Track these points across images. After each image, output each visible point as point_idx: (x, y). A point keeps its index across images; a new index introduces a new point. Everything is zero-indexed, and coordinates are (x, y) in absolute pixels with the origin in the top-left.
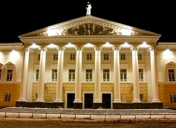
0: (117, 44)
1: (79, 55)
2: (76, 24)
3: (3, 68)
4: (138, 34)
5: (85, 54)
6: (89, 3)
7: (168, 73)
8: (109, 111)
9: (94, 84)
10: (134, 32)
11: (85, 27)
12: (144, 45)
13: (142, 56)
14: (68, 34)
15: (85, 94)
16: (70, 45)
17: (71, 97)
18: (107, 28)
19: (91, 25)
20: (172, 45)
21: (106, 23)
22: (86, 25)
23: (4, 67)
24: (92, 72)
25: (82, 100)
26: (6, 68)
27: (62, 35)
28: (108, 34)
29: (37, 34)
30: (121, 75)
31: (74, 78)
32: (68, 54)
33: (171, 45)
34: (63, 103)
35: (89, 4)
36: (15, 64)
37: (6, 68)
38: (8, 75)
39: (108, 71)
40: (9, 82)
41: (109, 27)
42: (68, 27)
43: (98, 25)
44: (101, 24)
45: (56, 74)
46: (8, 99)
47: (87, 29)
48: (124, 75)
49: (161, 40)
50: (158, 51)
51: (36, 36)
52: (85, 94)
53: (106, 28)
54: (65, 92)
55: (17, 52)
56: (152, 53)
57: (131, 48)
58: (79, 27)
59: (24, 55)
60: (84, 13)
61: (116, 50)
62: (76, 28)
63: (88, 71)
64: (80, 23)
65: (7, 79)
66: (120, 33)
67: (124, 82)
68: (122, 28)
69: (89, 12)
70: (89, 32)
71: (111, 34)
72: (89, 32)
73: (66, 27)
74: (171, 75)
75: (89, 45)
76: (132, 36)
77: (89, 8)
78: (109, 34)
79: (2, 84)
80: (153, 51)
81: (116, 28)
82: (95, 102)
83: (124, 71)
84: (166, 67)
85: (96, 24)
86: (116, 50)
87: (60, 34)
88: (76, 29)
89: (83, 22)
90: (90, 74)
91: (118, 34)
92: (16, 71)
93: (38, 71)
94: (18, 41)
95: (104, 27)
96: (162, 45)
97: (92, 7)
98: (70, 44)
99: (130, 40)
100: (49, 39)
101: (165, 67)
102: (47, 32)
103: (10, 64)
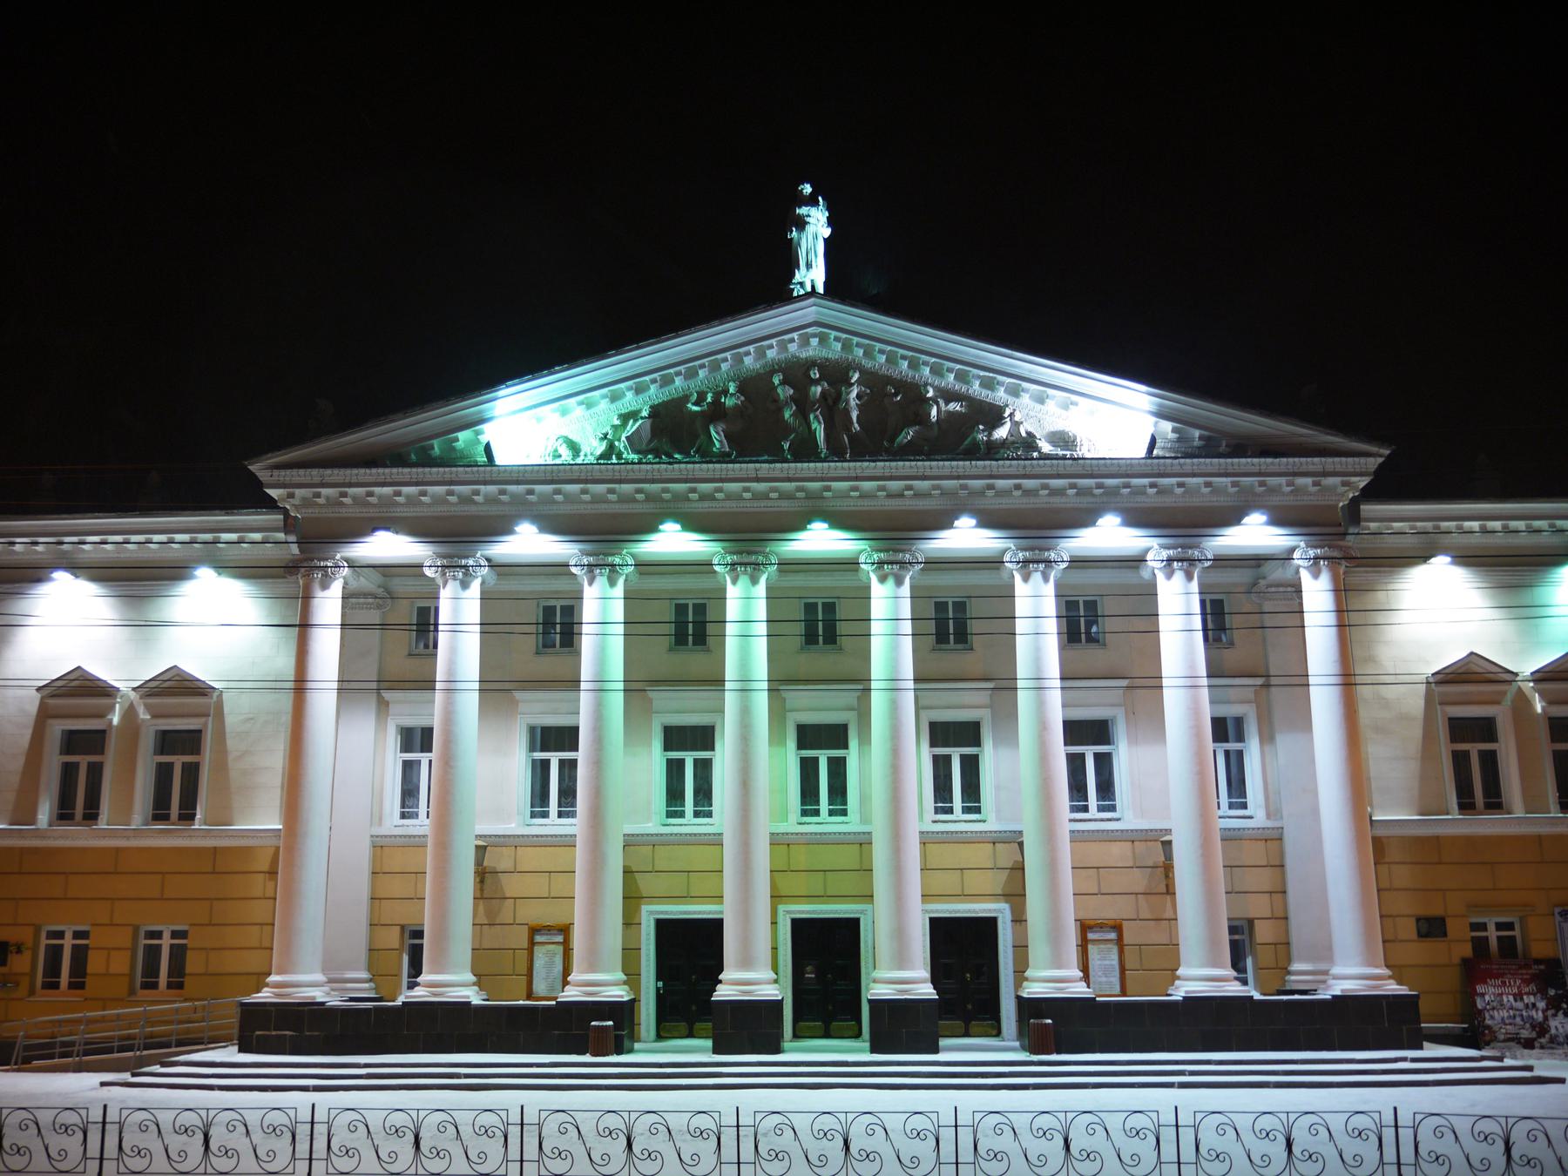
2: (715, 367)
3: (116, 720)
4: (1197, 443)
6: (807, 189)
7: (1445, 749)
10: (1167, 426)
11: (785, 392)
13: (1244, 619)
16: (672, 541)
19: (836, 374)
21: (949, 362)
22: (797, 373)
23: (130, 712)
26: (143, 715)
34: (633, 1001)
35: (812, 201)
37: (143, 715)
39: (968, 733)
41: (976, 389)
42: (655, 394)
46: (163, 978)
47: (803, 405)
49: (1384, 487)
53: (950, 396)
56: (1317, 594)
58: (740, 390)
62: (716, 402)
63: (676, 738)
68: (1074, 398)
69: (812, 274)
71: (993, 450)
73: (639, 390)
75: (820, 540)
76: (1150, 467)
78: (973, 452)
83: (954, 736)
85: (868, 364)
88: (716, 412)
92: (231, 743)
95: (931, 394)
96: (1395, 519)
97: (830, 222)
103: (177, 687)
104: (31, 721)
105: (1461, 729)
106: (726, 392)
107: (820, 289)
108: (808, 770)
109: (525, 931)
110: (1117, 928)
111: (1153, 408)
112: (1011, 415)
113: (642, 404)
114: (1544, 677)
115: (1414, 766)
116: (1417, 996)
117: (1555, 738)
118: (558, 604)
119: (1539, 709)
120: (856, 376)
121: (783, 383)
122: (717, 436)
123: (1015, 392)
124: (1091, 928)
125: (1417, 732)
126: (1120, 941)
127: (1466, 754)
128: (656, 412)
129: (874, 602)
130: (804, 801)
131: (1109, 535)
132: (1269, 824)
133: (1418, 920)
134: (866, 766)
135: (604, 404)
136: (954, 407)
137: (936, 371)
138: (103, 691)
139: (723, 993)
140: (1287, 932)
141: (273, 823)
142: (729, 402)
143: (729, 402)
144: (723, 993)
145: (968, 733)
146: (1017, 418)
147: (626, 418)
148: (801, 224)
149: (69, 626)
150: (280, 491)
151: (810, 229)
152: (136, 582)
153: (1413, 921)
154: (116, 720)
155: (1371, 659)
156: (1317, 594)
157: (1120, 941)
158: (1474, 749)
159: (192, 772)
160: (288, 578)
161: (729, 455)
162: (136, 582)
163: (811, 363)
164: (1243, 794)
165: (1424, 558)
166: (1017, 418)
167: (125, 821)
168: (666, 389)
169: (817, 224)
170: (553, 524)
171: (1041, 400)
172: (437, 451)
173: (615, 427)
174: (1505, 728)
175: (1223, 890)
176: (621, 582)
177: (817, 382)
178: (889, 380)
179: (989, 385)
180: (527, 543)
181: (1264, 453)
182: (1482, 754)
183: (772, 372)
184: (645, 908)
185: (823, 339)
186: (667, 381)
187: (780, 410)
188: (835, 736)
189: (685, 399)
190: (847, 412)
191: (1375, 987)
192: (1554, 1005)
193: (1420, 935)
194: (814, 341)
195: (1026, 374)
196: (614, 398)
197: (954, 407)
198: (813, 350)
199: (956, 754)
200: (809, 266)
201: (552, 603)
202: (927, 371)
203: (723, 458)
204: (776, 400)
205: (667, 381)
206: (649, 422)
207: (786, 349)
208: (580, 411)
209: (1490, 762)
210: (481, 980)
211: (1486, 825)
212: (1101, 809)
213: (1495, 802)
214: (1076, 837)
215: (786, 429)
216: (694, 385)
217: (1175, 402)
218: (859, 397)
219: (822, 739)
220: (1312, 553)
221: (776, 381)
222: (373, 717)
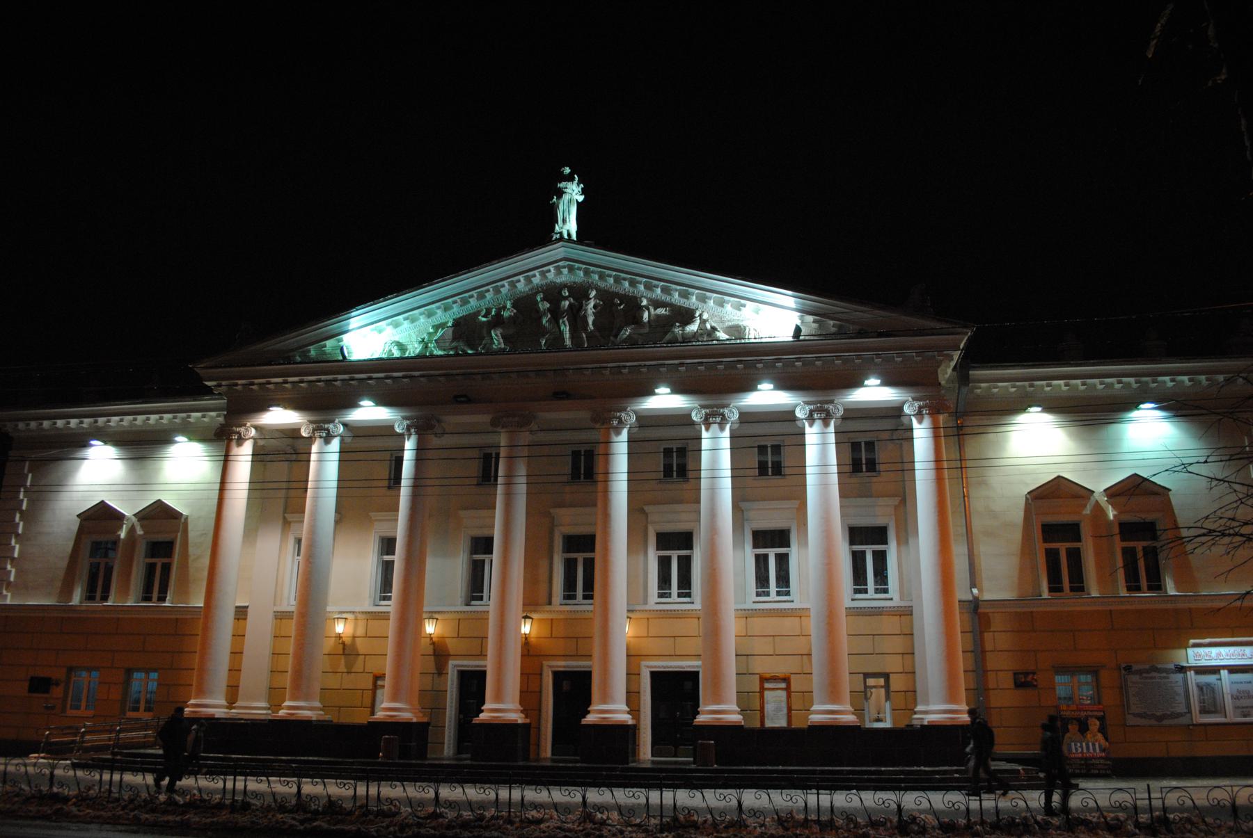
1: (715, 450)
2: (497, 291)
3: (123, 535)
4: (833, 330)
5: (747, 442)
6: (567, 170)
7: (1040, 547)
8: (363, 764)
9: (799, 614)
10: (810, 318)
12: (873, 392)
13: (870, 453)
14: (455, 348)
15: (652, 673)
16: (873, 392)
17: (575, 689)
19: (580, 293)
20: (1062, 382)
21: (655, 282)
22: (553, 293)
23: (132, 530)
24: (885, 542)
26: (140, 532)
27: (420, 357)
28: (668, 337)
29: (293, 350)
30: (858, 559)
31: (685, 582)
32: (470, 453)
33: (1160, 378)
34: (526, 727)
35: (570, 178)
36: (185, 512)
37: (140, 532)
38: (151, 569)
39: (877, 535)
41: (676, 298)
42: (457, 311)
43: (613, 289)
44: (617, 280)
47: (556, 313)
48: (584, 571)
49: (976, 356)
50: (966, 421)
51: (289, 361)
52: (652, 673)
53: (657, 304)
54: (446, 663)
55: (1048, 418)
56: (922, 436)
57: (907, 410)
58: (514, 306)
59: (226, 462)
60: (540, 230)
61: (715, 427)
62: (498, 314)
63: (667, 540)
64: (521, 286)
65: (473, 591)
66: (737, 331)
67: (871, 598)
68: (743, 302)
70: (567, 335)
71: (687, 339)
72: (567, 335)
73: (446, 309)
74: (1140, 554)
75: (279, 417)
76: (798, 346)
80: (927, 422)
81: (711, 303)
83: (866, 536)
85: (602, 284)
86: (715, 427)
87: (414, 349)
88: (498, 321)
89: (537, 280)
90: (874, 552)
91: (722, 335)
92: (191, 550)
94: (195, 389)
95: (645, 302)
96: (995, 381)
97: (584, 192)
98: (663, 390)
99: (790, 364)
100: (269, 383)
101: (1022, 514)
102: (344, 337)
103: (160, 514)
104: (73, 536)
105: (1051, 532)
106: (504, 308)
107: (574, 237)
108: (761, 561)
109: (371, 677)
110: (786, 680)
111: (799, 307)
112: (701, 315)
113: (448, 318)
114: (1114, 493)
115: (1015, 561)
116: (428, 724)
118: (583, 449)
119: (1111, 517)
120: (593, 293)
121: (543, 299)
123: (703, 300)
124: (768, 680)
125: (1018, 536)
126: (788, 689)
127: (1057, 552)
128: (457, 323)
129: (728, 446)
130: (660, 588)
131: (766, 396)
132: (903, 604)
134: (804, 559)
135: (422, 319)
136: (661, 311)
137: (649, 287)
138: (117, 517)
139: (701, 719)
140: (914, 681)
141: (200, 603)
142: (506, 314)
143: (506, 314)
144: (701, 719)
145: (877, 535)
146: (705, 316)
147: (437, 327)
148: (560, 193)
149: (98, 473)
150: (214, 383)
151: (566, 197)
152: (141, 447)
153: (1010, 675)
154: (123, 535)
155: (983, 483)
156: (922, 436)
157: (788, 689)
158: (1063, 547)
159: (167, 568)
160: (222, 438)
161: (504, 350)
162: (141, 447)
163: (564, 286)
164: (788, 585)
165: (1022, 409)
166: (705, 316)
167: (126, 598)
168: (464, 308)
169: (574, 192)
171: (721, 304)
172: (313, 353)
173: (430, 334)
174: (1086, 531)
175: (960, 649)
176: (728, 427)
177: (566, 298)
179: (685, 295)
180: (368, 412)
181: (880, 335)
182: (1069, 551)
183: (537, 293)
184: (451, 663)
185: (571, 269)
186: (465, 302)
187: (540, 318)
188: (779, 538)
189: (478, 313)
190: (585, 317)
192: (5, 773)
194: (565, 271)
195: (709, 287)
196: (430, 315)
197: (661, 311)
198: (565, 277)
199: (869, 550)
200: (564, 221)
201: (489, 451)
202: (642, 287)
204: (538, 311)
205: (465, 302)
206: (451, 330)
207: (546, 277)
208: (406, 324)
209: (1075, 557)
211: (1069, 602)
212: (877, 591)
213: (1078, 584)
214: (854, 612)
215: (542, 331)
216: (483, 304)
217: (812, 302)
218: (595, 307)
219: (773, 539)
220: (917, 404)
221: (539, 299)
222: (279, 531)
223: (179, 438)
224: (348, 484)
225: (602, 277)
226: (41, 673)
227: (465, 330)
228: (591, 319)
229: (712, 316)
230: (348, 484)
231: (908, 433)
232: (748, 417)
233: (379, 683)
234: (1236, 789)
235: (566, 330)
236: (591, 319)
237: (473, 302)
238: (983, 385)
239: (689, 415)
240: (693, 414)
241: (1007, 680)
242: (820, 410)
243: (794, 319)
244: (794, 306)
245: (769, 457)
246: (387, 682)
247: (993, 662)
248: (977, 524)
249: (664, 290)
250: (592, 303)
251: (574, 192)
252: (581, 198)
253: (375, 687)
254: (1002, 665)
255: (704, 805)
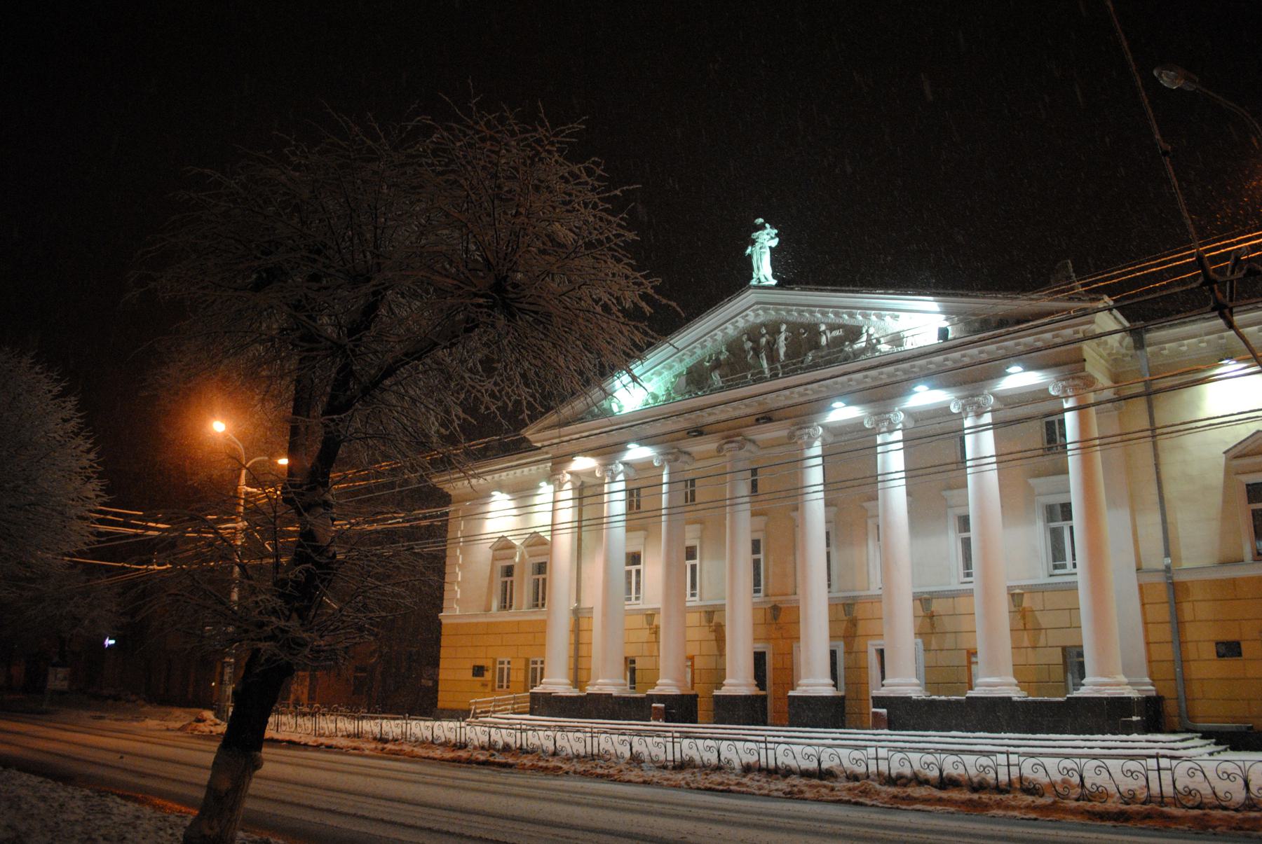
0: (882, 393)
3: (517, 560)
11: (749, 345)
12: (1019, 379)
13: (1034, 439)
16: (1019, 379)
18: (839, 327)
19: (774, 330)
21: (826, 307)
22: (753, 333)
23: (522, 556)
25: (835, 685)
35: (762, 227)
40: (506, 616)
43: (799, 320)
44: (800, 313)
45: (1071, 528)
46: (505, 684)
47: (756, 351)
53: (832, 327)
62: (717, 359)
64: (731, 330)
66: (896, 340)
69: (763, 270)
71: (856, 355)
73: (681, 361)
75: (583, 463)
76: (946, 346)
77: (764, 246)
79: (519, 622)
82: (440, 705)
84: (1229, 472)
85: (790, 319)
88: (717, 365)
91: (884, 348)
93: (964, 523)
95: (823, 328)
113: (680, 368)
116: (843, 698)
117: (1251, 500)
120: (784, 327)
122: (716, 376)
125: (1217, 498)
128: (690, 371)
133: (1217, 644)
136: (836, 333)
137: (824, 314)
138: (512, 547)
143: (722, 357)
152: (523, 493)
162: (523, 493)
163: (763, 325)
169: (766, 239)
170: (643, 441)
171: (880, 317)
178: (802, 325)
185: (765, 310)
189: (703, 360)
191: (1097, 691)
193: (1220, 655)
194: (761, 312)
197: (836, 333)
203: (721, 389)
210: (1021, 683)
215: (748, 367)
216: (707, 351)
223: (1231, 367)
224: (915, 473)
225: (789, 312)
226: (480, 663)
227: (696, 379)
228: (782, 351)
229: (877, 330)
230: (915, 473)
231: (424, 516)
232: (914, 415)
233: (974, 659)
234: (1248, 764)
235: (765, 364)
236: (782, 351)
237: (699, 352)
238: (1167, 346)
239: (862, 423)
240: (1051, 389)
241: (1209, 651)
242: (971, 404)
243: (941, 321)
244: (938, 309)
245: (936, 451)
246: (981, 657)
247: (1192, 633)
248: (1170, 490)
249: (836, 314)
250: (783, 336)
251: (766, 239)
252: (774, 243)
253: (970, 663)
254: (1202, 641)
255: (1047, 780)
